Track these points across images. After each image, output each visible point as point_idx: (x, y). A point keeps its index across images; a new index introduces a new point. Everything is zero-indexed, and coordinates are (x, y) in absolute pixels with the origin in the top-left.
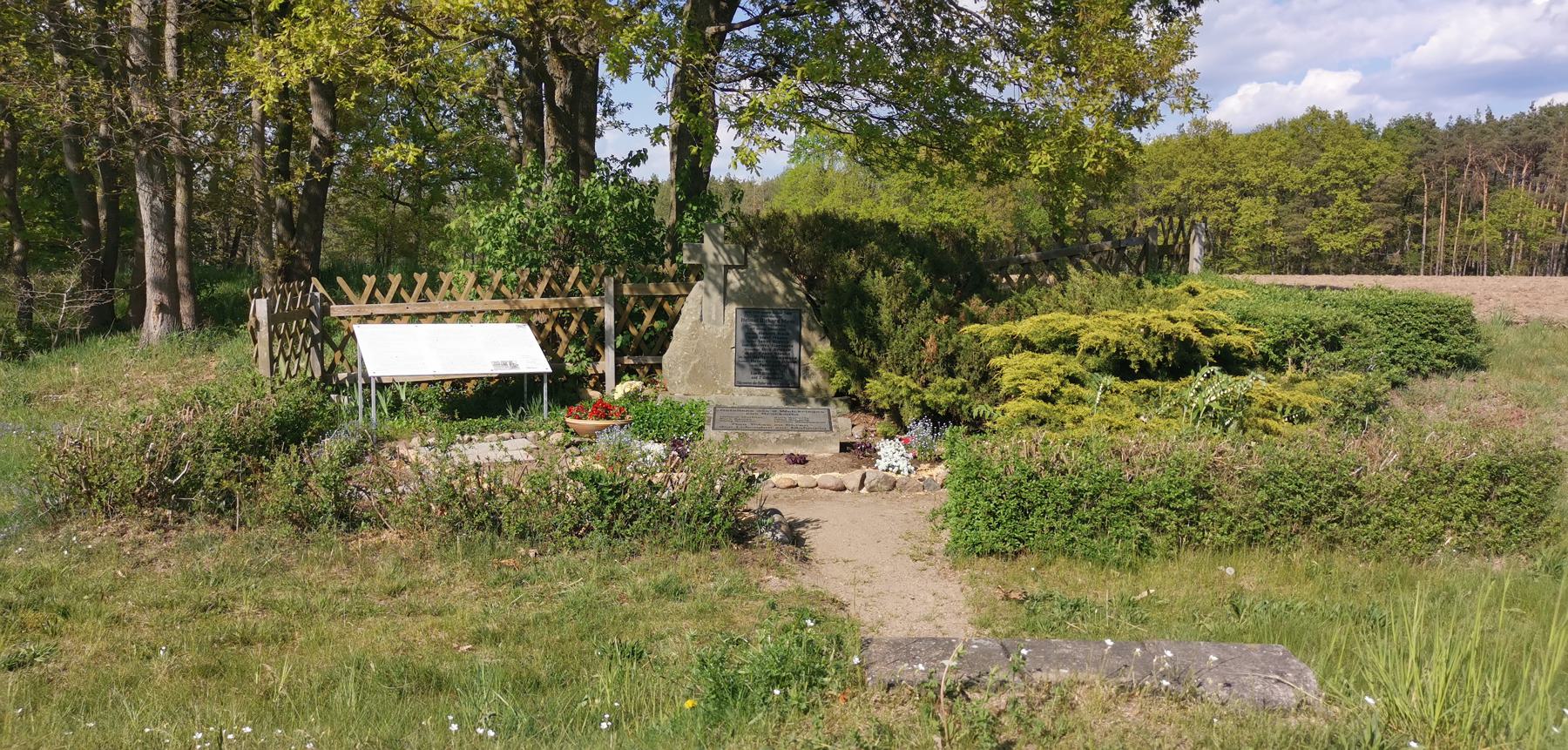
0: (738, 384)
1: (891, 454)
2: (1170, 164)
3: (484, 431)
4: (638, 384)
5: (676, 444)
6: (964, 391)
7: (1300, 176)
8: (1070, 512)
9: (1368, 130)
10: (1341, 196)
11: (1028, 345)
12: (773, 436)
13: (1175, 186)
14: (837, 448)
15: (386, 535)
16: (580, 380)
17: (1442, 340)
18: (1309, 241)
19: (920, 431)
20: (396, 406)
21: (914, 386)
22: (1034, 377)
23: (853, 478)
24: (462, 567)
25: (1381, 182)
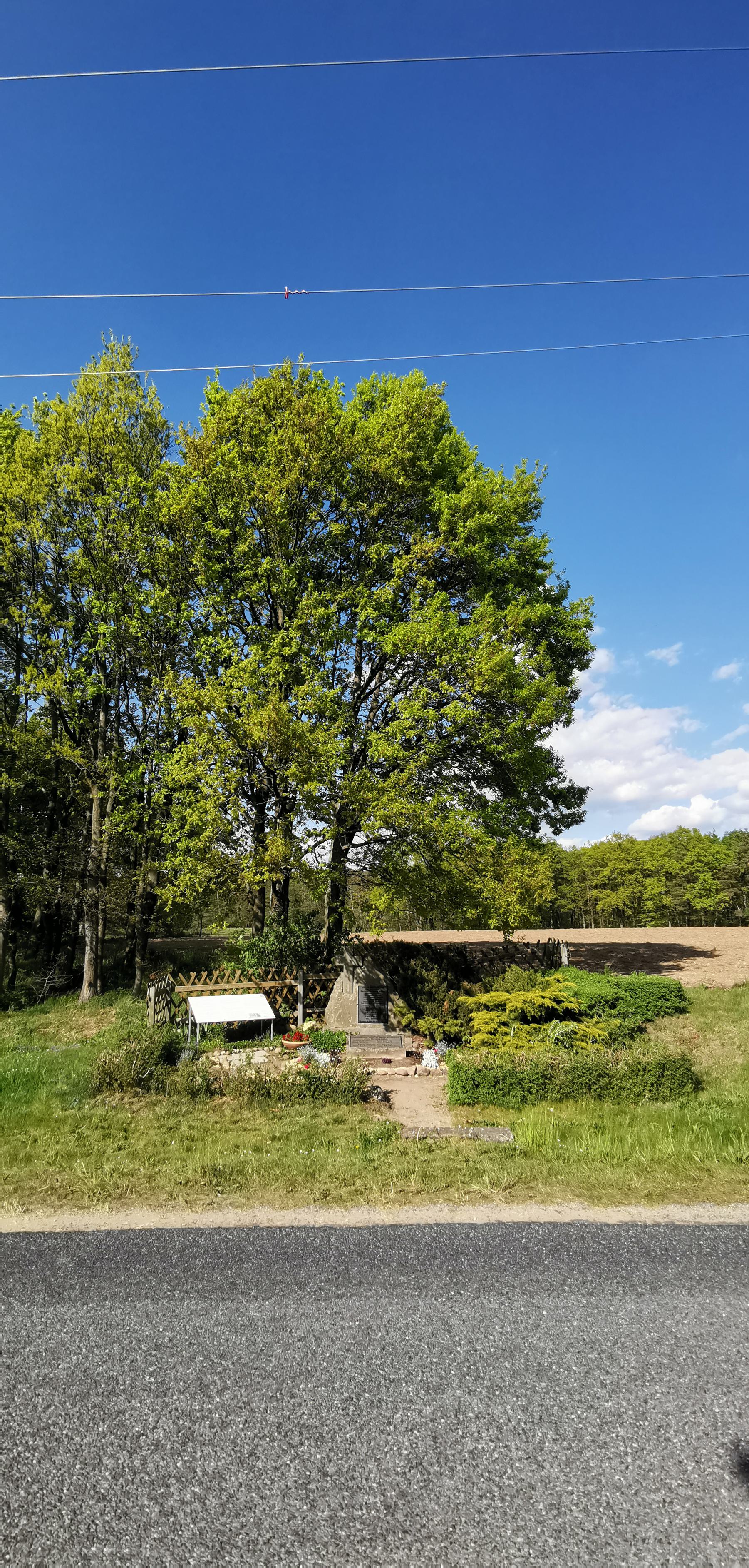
0: (360, 1022)
1: (429, 1057)
2: (603, 859)
3: (245, 1047)
4: (314, 1022)
5: (333, 1054)
6: (462, 1026)
7: (677, 866)
8: (494, 1086)
9: (714, 840)
10: (702, 876)
11: (487, 1008)
12: (376, 1050)
13: (606, 872)
14: (405, 1055)
15: (224, 1099)
16: (287, 1020)
17: (667, 1000)
18: (688, 903)
19: (441, 1046)
20: (204, 1035)
21: (440, 1024)
22: (486, 1023)
23: (411, 1070)
24: (258, 1112)
25: (724, 868)
